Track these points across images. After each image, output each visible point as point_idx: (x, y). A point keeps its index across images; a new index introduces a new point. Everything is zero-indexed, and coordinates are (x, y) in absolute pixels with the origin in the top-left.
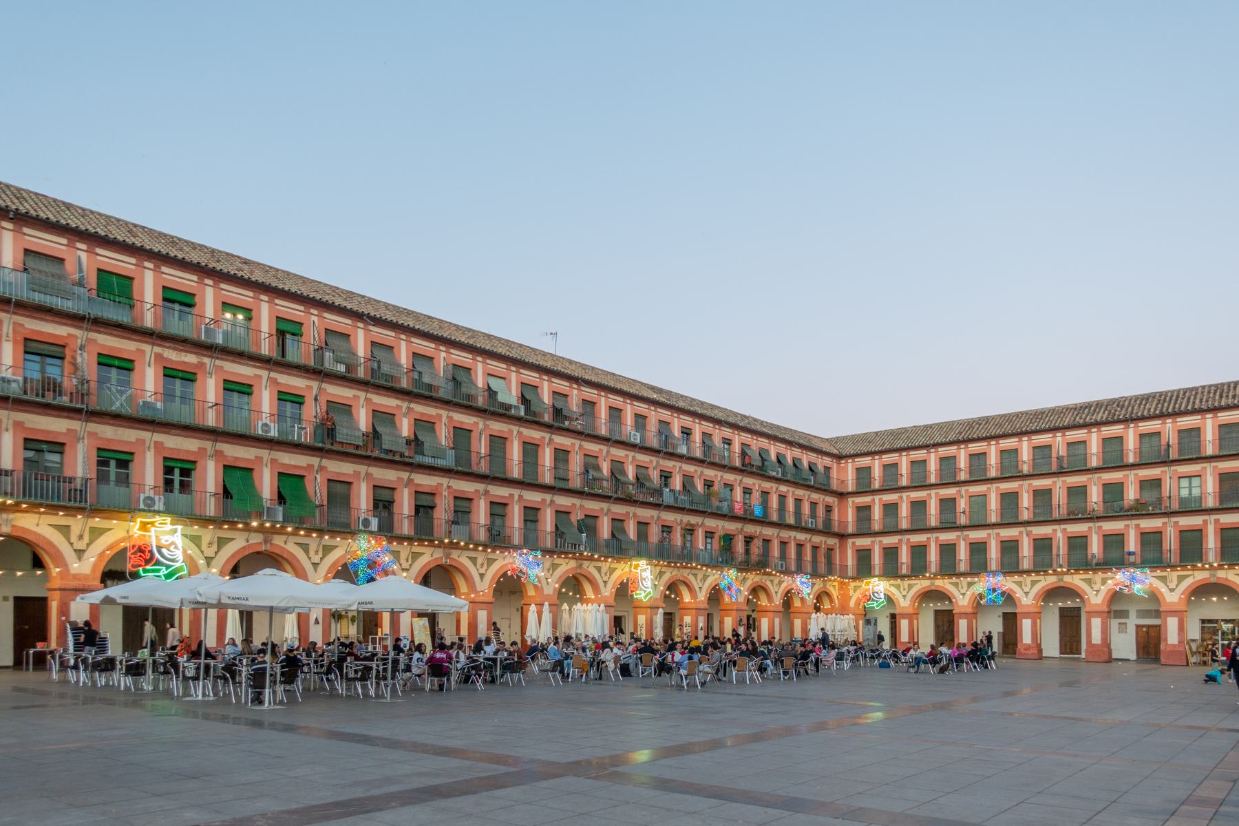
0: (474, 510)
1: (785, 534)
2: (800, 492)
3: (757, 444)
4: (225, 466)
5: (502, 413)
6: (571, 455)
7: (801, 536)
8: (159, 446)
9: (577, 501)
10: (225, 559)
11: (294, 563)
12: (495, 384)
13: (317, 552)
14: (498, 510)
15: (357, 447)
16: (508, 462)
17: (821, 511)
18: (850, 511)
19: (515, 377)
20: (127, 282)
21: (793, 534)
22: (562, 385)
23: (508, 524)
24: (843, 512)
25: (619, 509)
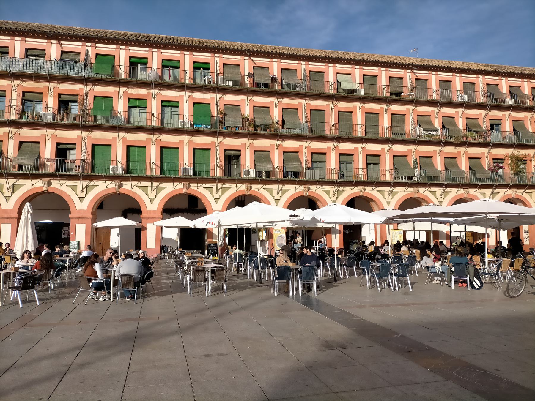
0: (355, 162)
5: (350, 96)
8: (124, 140)
11: (378, 203)
12: (340, 78)
14: (373, 160)
15: (238, 128)
16: (354, 127)
19: (358, 72)
20: (448, 83)
25: (450, 150)
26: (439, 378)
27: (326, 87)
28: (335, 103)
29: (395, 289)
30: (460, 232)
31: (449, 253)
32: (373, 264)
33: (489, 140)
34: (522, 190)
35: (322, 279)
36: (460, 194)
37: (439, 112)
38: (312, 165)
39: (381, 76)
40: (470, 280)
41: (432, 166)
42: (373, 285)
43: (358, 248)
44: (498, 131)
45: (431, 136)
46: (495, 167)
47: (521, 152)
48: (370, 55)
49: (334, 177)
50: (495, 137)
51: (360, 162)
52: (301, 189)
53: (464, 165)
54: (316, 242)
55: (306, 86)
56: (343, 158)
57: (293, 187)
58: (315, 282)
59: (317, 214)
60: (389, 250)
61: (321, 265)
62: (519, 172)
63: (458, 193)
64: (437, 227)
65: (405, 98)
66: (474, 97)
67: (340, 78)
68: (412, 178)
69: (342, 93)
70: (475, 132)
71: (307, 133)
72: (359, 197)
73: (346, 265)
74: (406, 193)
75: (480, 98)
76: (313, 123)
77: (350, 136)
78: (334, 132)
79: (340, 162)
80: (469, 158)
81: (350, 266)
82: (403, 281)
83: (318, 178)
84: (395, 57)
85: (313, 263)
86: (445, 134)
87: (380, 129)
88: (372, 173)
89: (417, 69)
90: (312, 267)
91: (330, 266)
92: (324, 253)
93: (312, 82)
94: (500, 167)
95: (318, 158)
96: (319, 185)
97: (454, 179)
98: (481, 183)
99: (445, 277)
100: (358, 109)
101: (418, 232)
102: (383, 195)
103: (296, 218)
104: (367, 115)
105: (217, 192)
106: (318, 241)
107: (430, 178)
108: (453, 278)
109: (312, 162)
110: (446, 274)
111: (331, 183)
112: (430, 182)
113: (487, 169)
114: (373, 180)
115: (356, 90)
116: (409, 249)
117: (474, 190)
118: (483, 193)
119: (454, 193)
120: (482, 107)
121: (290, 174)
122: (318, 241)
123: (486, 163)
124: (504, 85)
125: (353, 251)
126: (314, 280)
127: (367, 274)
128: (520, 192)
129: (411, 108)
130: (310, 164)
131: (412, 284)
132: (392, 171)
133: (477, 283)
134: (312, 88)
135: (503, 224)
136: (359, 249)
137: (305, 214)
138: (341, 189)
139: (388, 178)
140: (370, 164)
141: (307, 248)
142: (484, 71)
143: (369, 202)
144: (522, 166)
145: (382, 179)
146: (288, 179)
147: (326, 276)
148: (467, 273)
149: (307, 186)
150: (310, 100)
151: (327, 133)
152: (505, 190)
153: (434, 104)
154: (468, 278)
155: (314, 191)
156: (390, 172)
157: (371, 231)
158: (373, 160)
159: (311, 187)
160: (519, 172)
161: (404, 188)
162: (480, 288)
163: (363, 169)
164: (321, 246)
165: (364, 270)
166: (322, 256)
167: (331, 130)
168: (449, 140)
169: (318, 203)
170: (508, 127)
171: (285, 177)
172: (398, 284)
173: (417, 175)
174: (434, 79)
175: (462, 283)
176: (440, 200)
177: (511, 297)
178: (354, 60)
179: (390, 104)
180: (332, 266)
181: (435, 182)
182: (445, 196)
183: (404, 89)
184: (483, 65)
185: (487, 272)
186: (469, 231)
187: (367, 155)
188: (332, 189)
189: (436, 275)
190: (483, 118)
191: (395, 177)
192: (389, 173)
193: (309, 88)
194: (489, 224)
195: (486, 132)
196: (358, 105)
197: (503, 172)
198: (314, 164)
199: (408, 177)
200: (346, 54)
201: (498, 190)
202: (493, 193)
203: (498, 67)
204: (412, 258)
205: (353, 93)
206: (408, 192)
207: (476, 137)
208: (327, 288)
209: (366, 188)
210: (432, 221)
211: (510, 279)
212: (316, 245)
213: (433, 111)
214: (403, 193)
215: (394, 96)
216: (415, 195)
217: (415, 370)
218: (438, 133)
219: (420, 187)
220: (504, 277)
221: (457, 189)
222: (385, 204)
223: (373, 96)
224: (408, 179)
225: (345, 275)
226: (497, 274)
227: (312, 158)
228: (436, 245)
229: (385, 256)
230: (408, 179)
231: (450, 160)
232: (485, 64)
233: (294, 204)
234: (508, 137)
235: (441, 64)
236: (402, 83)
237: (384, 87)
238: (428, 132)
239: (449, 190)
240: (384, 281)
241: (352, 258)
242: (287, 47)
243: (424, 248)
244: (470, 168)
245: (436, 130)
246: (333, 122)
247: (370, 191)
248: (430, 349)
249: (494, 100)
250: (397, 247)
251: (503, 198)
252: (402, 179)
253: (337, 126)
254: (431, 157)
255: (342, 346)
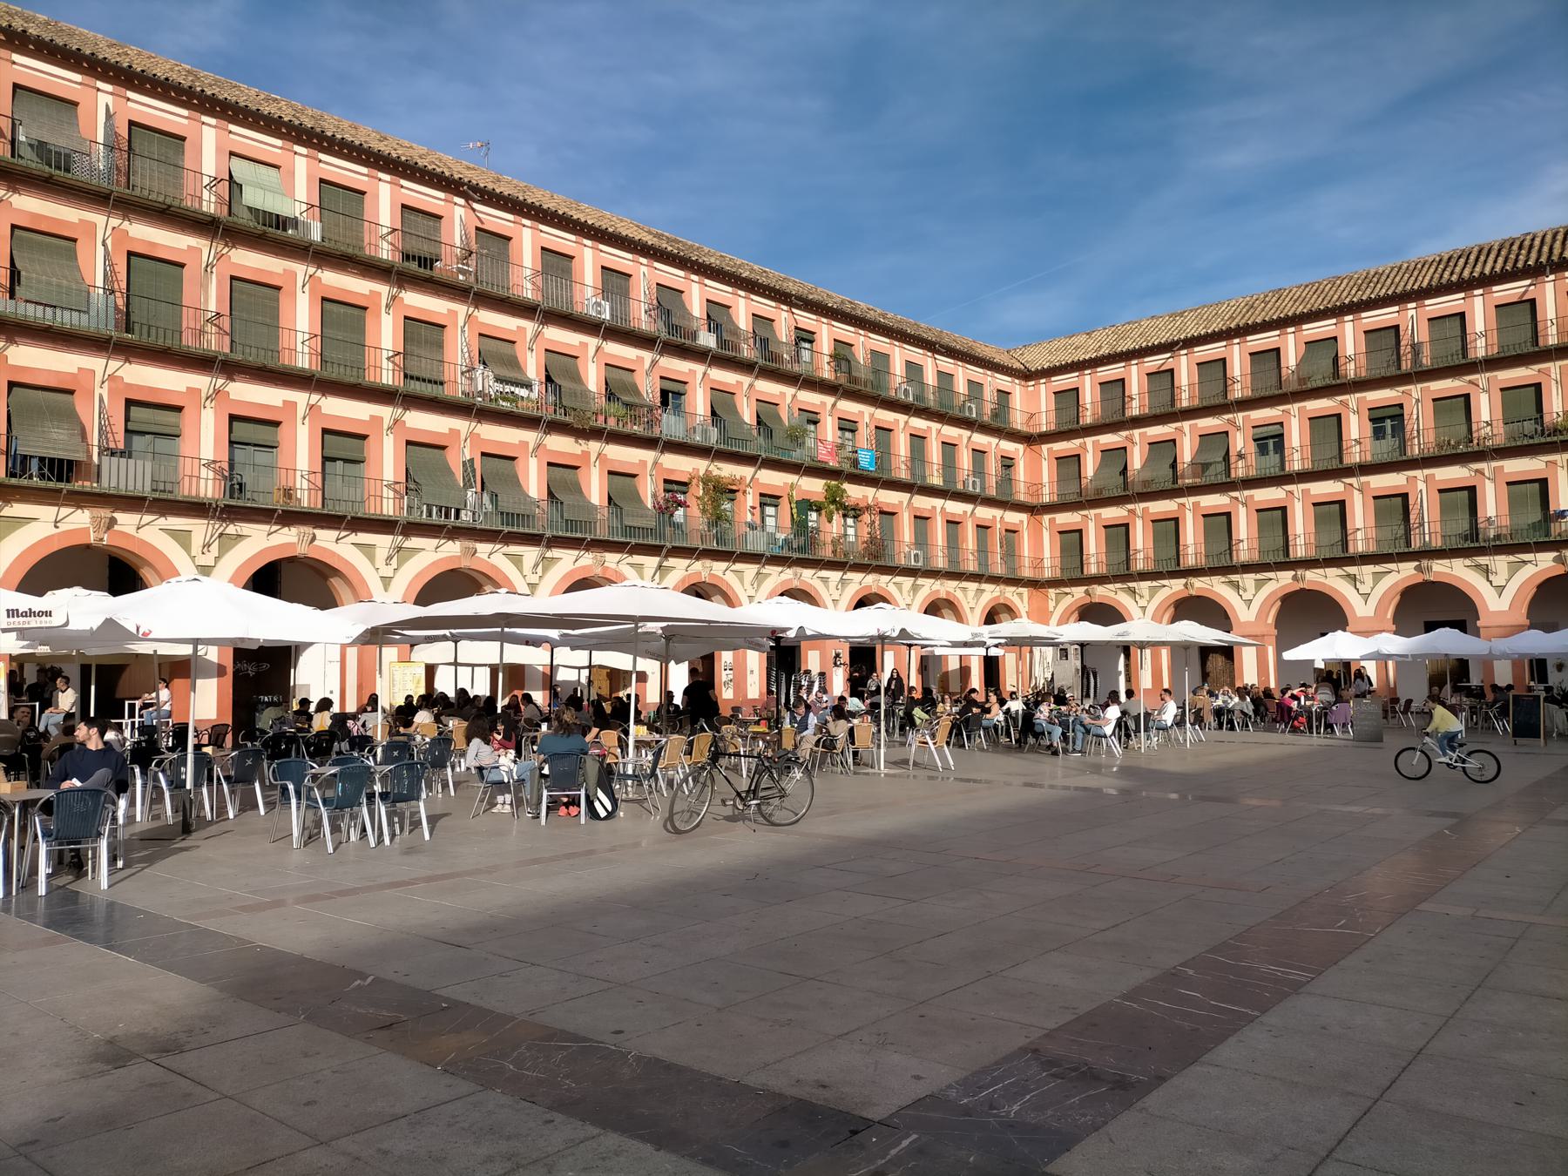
0: (284, 447)
1: (924, 503)
2: (951, 432)
3: (864, 344)
4: (408, 443)
5: (270, 233)
6: (448, 334)
7: (956, 508)
9: (997, 513)
10: (410, 578)
11: (355, 582)
12: (241, 169)
13: (207, 545)
17: (993, 466)
18: (1045, 464)
20: (564, 261)
21: (938, 502)
22: (766, 307)
23: (282, 462)
24: (1034, 469)
25: (561, 444)
26: (464, 1087)
27: (189, 185)
28: (219, 247)
29: (380, 840)
30: (579, 668)
31: (544, 727)
32: (317, 769)
33: (656, 432)
34: (724, 565)
35: (137, 829)
36: (583, 568)
37: (537, 335)
38: (128, 442)
39: (377, 196)
40: (587, 797)
41: (515, 482)
42: (312, 835)
43: (281, 721)
44: (678, 410)
45: (514, 398)
46: (667, 501)
47: (726, 471)
48: (345, 124)
49: (208, 487)
50: (670, 426)
51: (301, 453)
52: (79, 522)
53: (595, 490)
54: (132, 707)
55: (112, 168)
56: (242, 430)
57: (46, 513)
58: (103, 844)
59: (129, 609)
60: (377, 726)
61: (139, 782)
62: (719, 518)
63: (578, 564)
64: (517, 654)
65: (445, 276)
66: (627, 314)
67: (239, 168)
68: (458, 512)
69: (244, 219)
70: (626, 405)
71: (111, 330)
72: (292, 560)
73: (227, 778)
74: (440, 555)
75: (641, 318)
76: (135, 301)
77: (270, 364)
78: (214, 342)
79: (231, 443)
80: (610, 473)
81: (241, 778)
82: (407, 814)
83: (148, 488)
84: (423, 150)
85: (101, 775)
86: (551, 398)
87: (370, 356)
88: (337, 487)
89: (482, 202)
90: (96, 793)
91: (170, 783)
92: (155, 742)
93: (138, 163)
94: (680, 504)
95: (150, 421)
96: (149, 512)
97: (571, 524)
98: (633, 541)
99: (526, 793)
100: (299, 284)
101: (469, 668)
102: (372, 559)
103: (34, 622)
104: (328, 305)
105: (207, 545)
106: (138, 703)
107: (509, 517)
108: (545, 793)
109: (127, 431)
110: (528, 785)
111: (197, 508)
112: (506, 529)
113: (650, 505)
114: (340, 510)
115: (295, 223)
116: (437, 719)
117: (617, 556)
118: (638, 567)
119: (568, 561)
120: (643, 341)
121: (35, 464)
122: (138, 703)
123: (649, 490)
124: (697, 294)
125: (263, 732)
126: (99, 834)
127: (294, 801)
128: (719, 567)
129: (461, 309)
130: (120, 436)
131: (433, 820)
132: (402, 488)
133: (603, 803)
134: (136, 179)
135: (677, 646)
136: (283, 723)
137: (79, 610)
138: (231, 529)
139: (388, 508)
140: (334, 460)
141: (90, 722)
142: (652, 247)
143: (326, 578)
144: (727, 506)
145: (371, 510)
146: (24, 482)
147: (156, 817)
148: (581, 779)
149: (105, 513)
150: (125, 217)
151: (188, 341)
152: (687, 562)
153: (525, 309)
154: (583, 792)
155: (131, 530)
156: (395, 491)
157: (328, 665)
158: (341, 449)
159: (120, 516)
160: (719, 518)
161: (435, 542)
162: (610, 815)
163: (310, 473)
164: (150, 717)
165: (285, 789)
166: (145, 753)
167: (202, 332)
168: (560, 417)
169: (146, 573)
170: (699, 403)
171: (13, 475)
172: (391, 824)
173: (474, 506)
174: (529, 240)
175: (567, 805)
176: (531, 581)
177: (678, 832)
178: (289, 125)
179: (401, 287)
180: (177, 784)
181: (521, 530)
182: (545, 570)
183: (445, 251)
184: (649, 232)
185: (630, 772)
186: (601, 667)
187: (325, 431)
188: (199, 528)
189: (501, 787)
190: (648, 370)
191: (410, 508)
192: (391, 494)
193: (123, 179)
194: (643, 646)
195: (651, 409)
196: (301, 269)
197: (685, 516)
198: (136, 439)
199: (448, 510)
200: (267, 99)
201: (672, 561)
202: (660, 567)
203: (685, 244)
204: (443, 740)
205: (285, 229)
206: (449, 552)
207: (630, 420)
208: (150, 860)
209: (318, 532)
210: (503, 639)
211: (680, 786)
212: (132, 715)
213: (521, 330)
214: (432, 554)
215: (413, 266)
216: (465, 563)
217: (404, 1079)
218: (534, 395)
219: (322, 528)
220: (670, 783)
221: (576, 552)
222: (375, 585)
223: (350, 251)
224: (447, 516)
225: (222, 810)
226: (653, 774)
227: (127, 419)
228: (513, 706)
229: (363, 742)
230: (447, 516)
231: (562, 472)
232: (654, 230)
233: (43, 575)
234: (699, 430)
235: (549, 204)
236: (437, 230)
237: (385, 231)
238: (508, 388)
239: (555, 553)
240: (347, 817)
241: (257, 754)
242: (42, 17)
243: (478, 714)
244: (610, 499)
245: (528, 386)
246: (212, 307)
247: (329, 544)
248: (455, 1005)
249: (673, 328)
250: (404, 714)
251: (683, 580)
252: (430, 515)
253: (226, 323)
254: (513, 459)
255: (166, 1047)
